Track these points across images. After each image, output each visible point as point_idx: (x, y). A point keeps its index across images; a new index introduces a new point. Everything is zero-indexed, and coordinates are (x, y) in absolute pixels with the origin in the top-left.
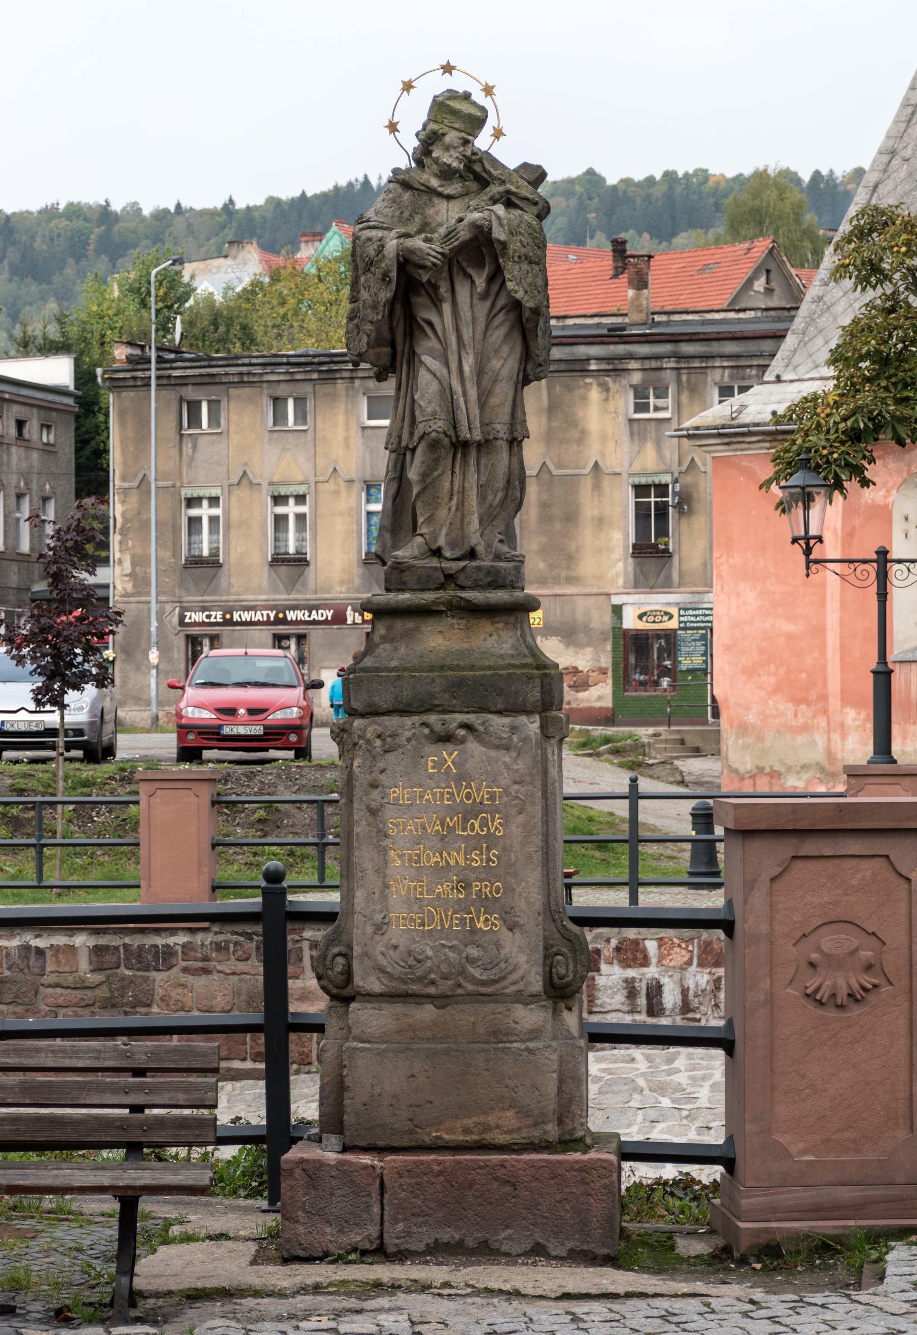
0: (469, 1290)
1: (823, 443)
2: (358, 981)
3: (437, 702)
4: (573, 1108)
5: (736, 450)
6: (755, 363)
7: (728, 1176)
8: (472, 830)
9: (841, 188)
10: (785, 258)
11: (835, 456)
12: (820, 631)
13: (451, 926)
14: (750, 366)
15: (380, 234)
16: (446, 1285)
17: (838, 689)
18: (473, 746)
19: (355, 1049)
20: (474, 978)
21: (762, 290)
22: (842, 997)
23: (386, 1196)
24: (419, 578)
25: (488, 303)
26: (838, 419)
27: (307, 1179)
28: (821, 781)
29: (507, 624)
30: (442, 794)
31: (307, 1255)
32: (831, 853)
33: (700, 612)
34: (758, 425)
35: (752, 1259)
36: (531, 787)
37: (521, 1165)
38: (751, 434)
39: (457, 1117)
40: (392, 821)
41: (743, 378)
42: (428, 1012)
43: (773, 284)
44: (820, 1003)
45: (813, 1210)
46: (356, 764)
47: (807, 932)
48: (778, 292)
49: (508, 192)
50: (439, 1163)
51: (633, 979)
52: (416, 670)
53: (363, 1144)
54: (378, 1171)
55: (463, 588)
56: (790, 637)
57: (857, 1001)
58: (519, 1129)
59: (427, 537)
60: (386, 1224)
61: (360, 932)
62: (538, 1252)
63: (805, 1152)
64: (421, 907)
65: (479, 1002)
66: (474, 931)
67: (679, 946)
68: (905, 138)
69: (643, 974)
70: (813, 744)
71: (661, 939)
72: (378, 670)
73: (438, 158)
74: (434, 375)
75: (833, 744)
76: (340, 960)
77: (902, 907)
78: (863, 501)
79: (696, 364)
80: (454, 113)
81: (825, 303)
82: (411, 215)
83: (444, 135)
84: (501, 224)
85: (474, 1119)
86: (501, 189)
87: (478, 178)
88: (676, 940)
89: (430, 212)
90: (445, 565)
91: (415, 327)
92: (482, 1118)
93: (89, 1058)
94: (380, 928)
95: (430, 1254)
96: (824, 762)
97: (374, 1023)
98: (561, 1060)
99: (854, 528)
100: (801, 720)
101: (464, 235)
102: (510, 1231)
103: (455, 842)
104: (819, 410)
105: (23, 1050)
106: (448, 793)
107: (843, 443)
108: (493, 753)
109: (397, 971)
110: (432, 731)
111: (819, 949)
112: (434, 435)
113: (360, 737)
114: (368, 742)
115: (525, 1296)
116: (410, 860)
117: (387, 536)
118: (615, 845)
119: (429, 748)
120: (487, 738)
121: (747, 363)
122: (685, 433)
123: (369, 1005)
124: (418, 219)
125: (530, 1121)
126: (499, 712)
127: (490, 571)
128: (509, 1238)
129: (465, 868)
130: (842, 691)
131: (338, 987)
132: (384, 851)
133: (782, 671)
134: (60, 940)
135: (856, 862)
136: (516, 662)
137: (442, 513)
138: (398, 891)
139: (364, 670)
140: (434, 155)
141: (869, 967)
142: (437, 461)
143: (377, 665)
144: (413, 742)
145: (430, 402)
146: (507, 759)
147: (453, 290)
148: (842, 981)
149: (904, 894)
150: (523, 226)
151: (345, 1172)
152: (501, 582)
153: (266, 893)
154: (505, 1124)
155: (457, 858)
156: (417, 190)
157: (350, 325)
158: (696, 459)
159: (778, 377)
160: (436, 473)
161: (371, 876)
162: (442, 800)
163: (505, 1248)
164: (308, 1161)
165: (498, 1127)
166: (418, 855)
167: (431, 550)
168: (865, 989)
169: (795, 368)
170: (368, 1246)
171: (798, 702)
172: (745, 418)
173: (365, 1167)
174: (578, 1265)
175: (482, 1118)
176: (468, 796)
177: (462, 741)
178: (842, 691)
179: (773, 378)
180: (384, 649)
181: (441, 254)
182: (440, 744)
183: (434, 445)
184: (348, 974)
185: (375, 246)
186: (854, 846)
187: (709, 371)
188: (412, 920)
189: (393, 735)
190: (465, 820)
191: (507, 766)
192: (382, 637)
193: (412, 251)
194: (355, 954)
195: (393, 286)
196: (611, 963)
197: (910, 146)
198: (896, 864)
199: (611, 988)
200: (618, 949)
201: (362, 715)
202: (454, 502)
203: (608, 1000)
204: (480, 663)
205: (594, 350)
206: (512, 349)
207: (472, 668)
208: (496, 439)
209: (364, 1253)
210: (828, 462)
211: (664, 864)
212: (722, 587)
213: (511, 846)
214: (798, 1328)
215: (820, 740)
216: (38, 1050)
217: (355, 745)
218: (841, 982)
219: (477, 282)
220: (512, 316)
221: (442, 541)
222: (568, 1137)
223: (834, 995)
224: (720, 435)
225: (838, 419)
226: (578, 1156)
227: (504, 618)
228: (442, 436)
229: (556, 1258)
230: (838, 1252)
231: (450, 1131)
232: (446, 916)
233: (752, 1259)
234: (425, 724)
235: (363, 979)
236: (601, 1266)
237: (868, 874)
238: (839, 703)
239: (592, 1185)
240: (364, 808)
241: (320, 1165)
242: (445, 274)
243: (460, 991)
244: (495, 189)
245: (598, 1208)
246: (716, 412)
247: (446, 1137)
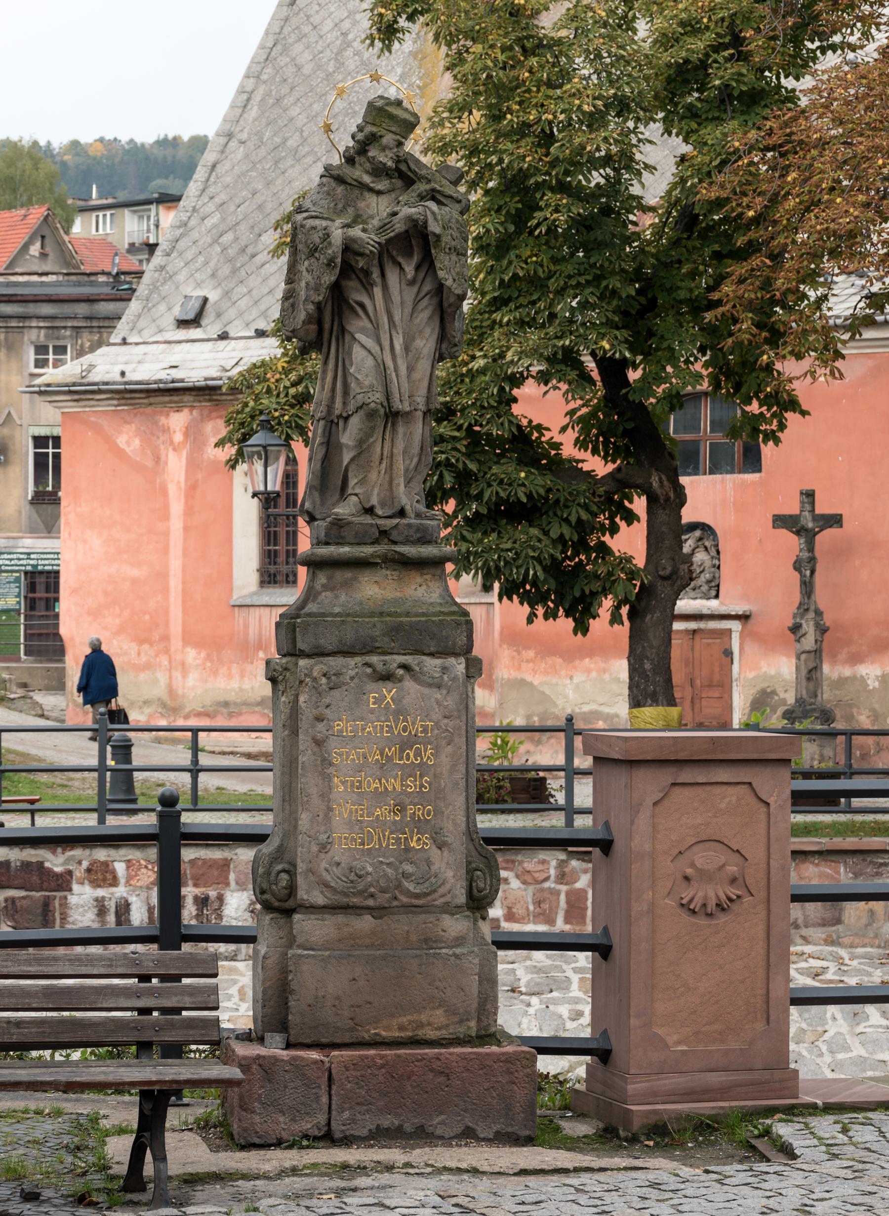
0: (429, 1170)
1: (275, 406)
2: (302, 894)
3: (377, 645)
4: (488, 1006)
5: (85, 406)
6: (70, 324)
7: (600, 1066)
8: (408, 759)
9: (58, 159)
10: (58, 225)
11: (286, 418)
12: (164, 576)
13: (388, 845)
14: (65, 327)
15: (324, 223)
16: (408, 1165)
17: (180, 630)
18: (409, 684)
19: (301, 956)
20: (409, 890)
21: (37, 254)
22: (711, 906)
23: (334, 1087)
24: (356, 534)
25: (415, 289)
26: (288, 384)
27: (263, 1073)
28: (162, 715)
29: (434, 575)
30: (382, 727)
31: (262, 1142)
32: (704, 781)
33: (15, 556)
34: (107, 383)
35: (643, 1138)
36: (458, 721)
37: (453, 1058)
38: (100, 392)
39: (393, 1016)
40: (337, 752)
41: (58, 338)
42: (367, 922)
43: (48, 250)
44: (694, 912)
45: (688, 1094)
46: (302, 699)
47: (682, 849)
48: (52, 256)
49: (433, 190)
50: (382, 1057)
51: (103, 898)
52: (358, 616)
53: (308, 1041)
54: (327, 1065)
55: (395, 543)
56: (135, 581)
57: (723, 909)
58: (447, 1026)
59: (361, 497)
60: (334, 1113)
61: (304, 853)
62: (468, 1135)
63: (679, 1043)
64: (361, 828)
65: (412, 912)
66: (408, 850)
67: (146, 867)
68: (241, 122)
69: (112, 894)
70: (156, 681)
71: (129, 861)
72: (323, 615)
73: (373, 158)
74: (369, 351)
75: (174, 682)
76: (284, 876)
77: (763, 827)
78: (205, 456)
79: (14, 324)
80: (392, 117)
81: (167, 272)
83: (381, 137)
84: (436, 219)
85: (409, 1017)
86: (428, 187)
87: (402, 175)
88: (143, 862)
89: (362, 205)
90: (380, 522)
91: (344, 308)
92: (415, 1017)
93: (103, 966)
94: (324, 847)
95: (373, 1138)
96: (165, 697)
97: (318, 932)
98: (481, 965)
99: (197, 481)
100: (144, 659)
101: (399, 227)
102: (443, 1117)
103: (392, 770)
104: (269, 376)
105: (43, 959)
107: (292, 406)
108: (426, 691)
109: (339, 885)
110: (374, 670)
111: (693, 865)
112: (373, 405)
113: (306, 675)
114: (315, 679)
115: (483, 1173)
116: (352, 786)
117: (316, 494)
118: (11, 774)
119: (371, 686)
120: (422, 678)
121: (63, 324)
122: (37, 389)
123: (313, 917)
124: (350, 210)
125: (456, 1019)
126: (431, 655)
127: (419, 529)
128: (442, 1123)
129: (401, 793)
130: (184, 632)
131: (280, 901)
132: (328, 778)
133: (126, 613)
134: (215, 854)
135: (725, 787)
136: (446, 610)
137: (373, 476)
138: (343, 812)
139: (309, 615)
140: (370, 154)
141: (733, 881)
142: (373, 429)
143: (321, 611)
144: (356, 680)
145: (367, 376)
146: (439, 696)
147: (383, 275)
148: (711, 893)
149: (763, 817)
150: (454, 221)
151: (297, 1067)
152: (429, 538)
153: (161, 816)
154: (435, 1022)
155: (393, 784)
156: (350, 184)
157: (286, 304)
158: (13, 413)
159: (124, 339)
160: (371, 440)
161: (316, 801)
162: (382, 732)
163: (439, 1132)
164: (264, 1057)
165: (429, 1024)
166: (360, 782)
168: (731, 900)
169: (140, 332)
170: (316, 1133)
171: (141, 642)
172: (94, 377)
173: (315, 1062)
174: (504, 1145)
175: (415, 1017)
176: (405, 730)
178: (184, 632)
179: (119, 341)
180: (326, 597)
181: (379, 243)
182: (381, 682)
183: (372, 415)
184: (292, 889)
185: (321, 235)
186: (723, 774)
187: (26, 330)
190: (402, 750)
191: (438, 703)
192: (323, 586)
193: (354, 240)
194: (299, 870)
196: (82, 884)
197: (246, 130)
198: (757, 790)
199: (82, 906)
200: (89, 870)
201: (309, 656)
202: (383, 466)
203: (79, 918)
204: (414, 610)
206: (433, 329)
207: (408, 614)
209: (316, 1138)
210: (279, 423)
211: (59, 792)
212: (70, 534)
213: (441, 774)
214: (783, 1192)
215: (162, 678)
216: (56, 959)
217: (301, 682)
218: (711, 894)
220: (435, 301)
221: (374, 501)
222: (484, 1032)
223: (704, 905)
224: (70, 392)
225: (288, 384)
226: (494, 1049)
227: (432, 571)
229: (484, 1139)
230: (716, 1130)
231: (388, 1028)
232: (384, 836)
233: (643, 1138)
235: (308, 893)
236: (523, 1146)
237: (734, 799)
238: (180, 643)
239: (516, 1074)
240: (310, 739)
241: (275, 1060)
242: (376, 262)
243: (395, 903)
244: (422, 187)
245: (520, 1094)
246: (68, 370)
247: (384, 1033)
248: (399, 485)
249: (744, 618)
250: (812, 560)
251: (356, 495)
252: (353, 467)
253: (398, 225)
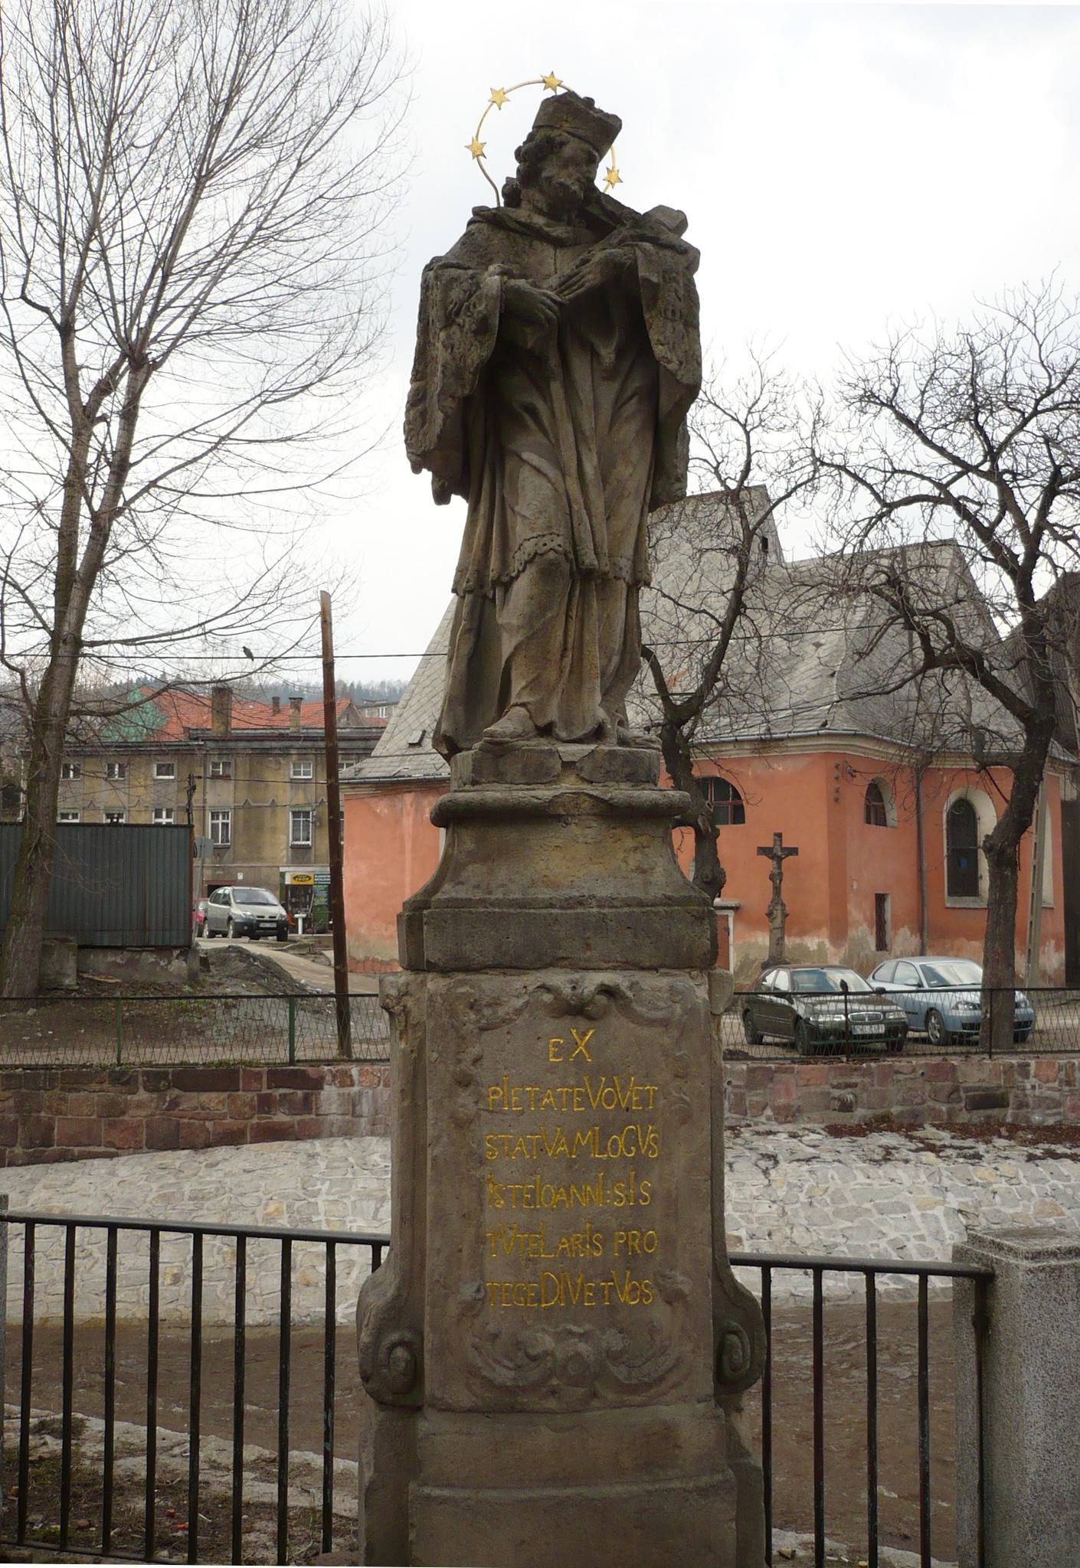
2: (430, 1386)
3: (561, 953)
25: (616, 385)
66: (613, 1308)
73: (549, 179)
76: (400, 1352)
83: (562, 144)
112: (552, 555)
127: (627, 760)
132: (480, 1186)
146: (666, 1041)
162: (570, 1105)
166: (533, 1192)
167: (537, 728)
176: (609, 1099)
177: (605, 1012)
180: (474, 872)
182: (567, 1020)
189: (495, 1003)
190: (605, 1135)
193: (518, 292)
194: (427, 1346)
195: (493, 342)
202: (568, 660)
205: (274, 744)
208: (617, 578)
219: (603, 352)
228: (562, 558)
232: (574, 1285)
234: (548, 989)
248: (592, 690)
249: (736, 909)
250: (781, 874)
251: (523, 705)
252: (519, 660)
253: (590, 277)
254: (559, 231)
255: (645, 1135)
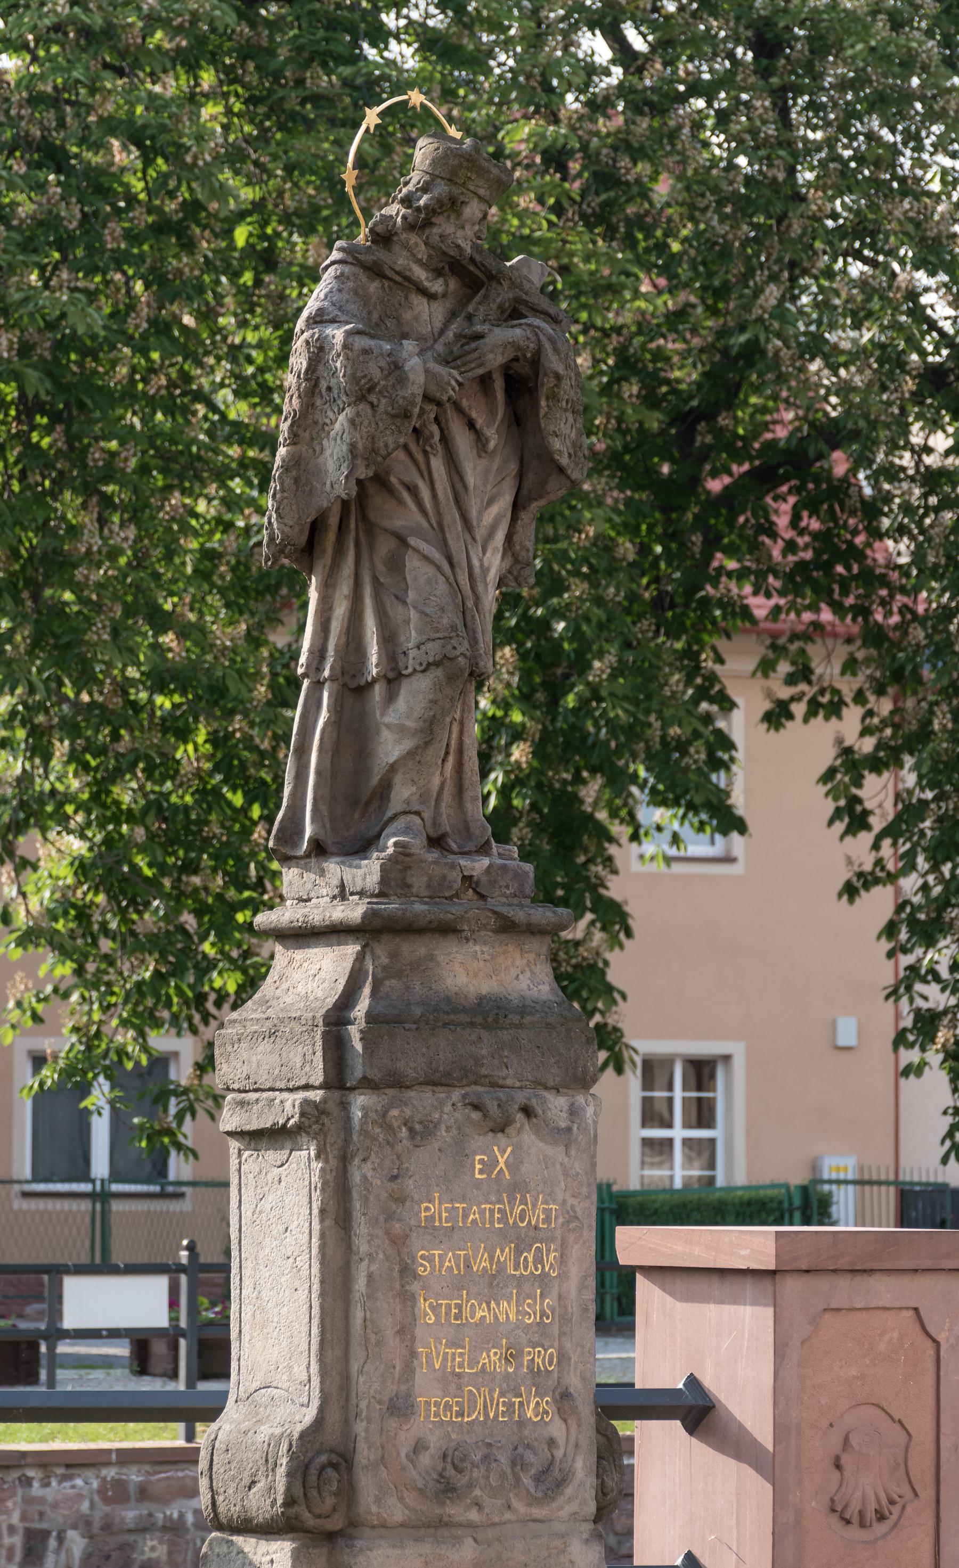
3: (484, 1071)
13: (496, 1416)
18: (528, 1138)
22: (870, 1515)
24: (430, 880)
30: (492, 1211)
44: (848, 1522)
76: (331, 1473)
82: (380, 318)
106: (500, 1210)
119: (478, 1141)
132: (408, 1299)
135: (885, 1315)
162: (492, 1222)
185: (383, 363)
188: (448, 1407)
190: (518, 1252)
243: (508, 1516)
254: (437, 287)
255: (548, 1251)
